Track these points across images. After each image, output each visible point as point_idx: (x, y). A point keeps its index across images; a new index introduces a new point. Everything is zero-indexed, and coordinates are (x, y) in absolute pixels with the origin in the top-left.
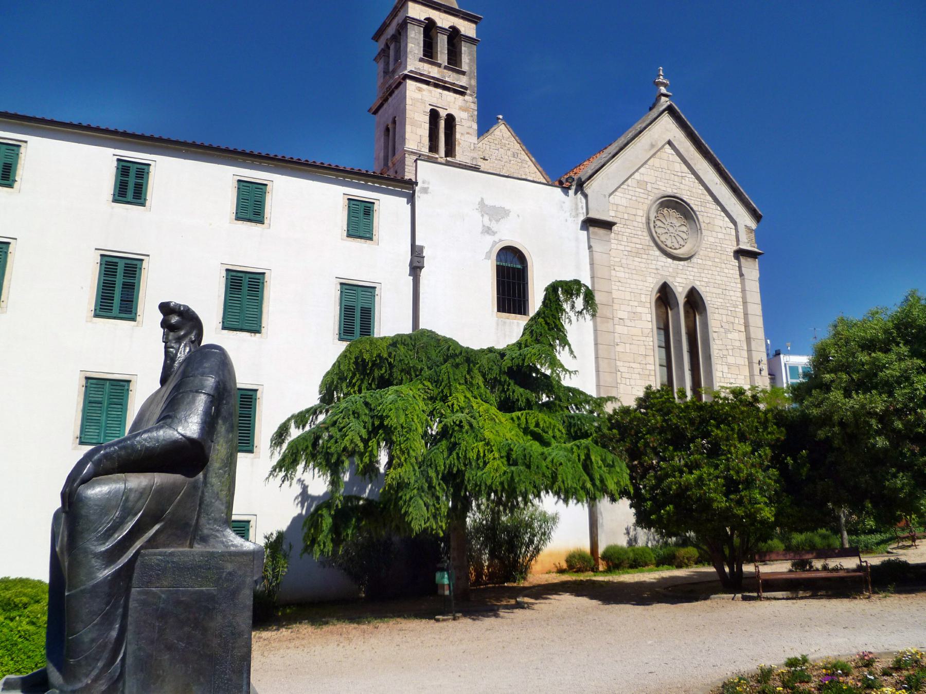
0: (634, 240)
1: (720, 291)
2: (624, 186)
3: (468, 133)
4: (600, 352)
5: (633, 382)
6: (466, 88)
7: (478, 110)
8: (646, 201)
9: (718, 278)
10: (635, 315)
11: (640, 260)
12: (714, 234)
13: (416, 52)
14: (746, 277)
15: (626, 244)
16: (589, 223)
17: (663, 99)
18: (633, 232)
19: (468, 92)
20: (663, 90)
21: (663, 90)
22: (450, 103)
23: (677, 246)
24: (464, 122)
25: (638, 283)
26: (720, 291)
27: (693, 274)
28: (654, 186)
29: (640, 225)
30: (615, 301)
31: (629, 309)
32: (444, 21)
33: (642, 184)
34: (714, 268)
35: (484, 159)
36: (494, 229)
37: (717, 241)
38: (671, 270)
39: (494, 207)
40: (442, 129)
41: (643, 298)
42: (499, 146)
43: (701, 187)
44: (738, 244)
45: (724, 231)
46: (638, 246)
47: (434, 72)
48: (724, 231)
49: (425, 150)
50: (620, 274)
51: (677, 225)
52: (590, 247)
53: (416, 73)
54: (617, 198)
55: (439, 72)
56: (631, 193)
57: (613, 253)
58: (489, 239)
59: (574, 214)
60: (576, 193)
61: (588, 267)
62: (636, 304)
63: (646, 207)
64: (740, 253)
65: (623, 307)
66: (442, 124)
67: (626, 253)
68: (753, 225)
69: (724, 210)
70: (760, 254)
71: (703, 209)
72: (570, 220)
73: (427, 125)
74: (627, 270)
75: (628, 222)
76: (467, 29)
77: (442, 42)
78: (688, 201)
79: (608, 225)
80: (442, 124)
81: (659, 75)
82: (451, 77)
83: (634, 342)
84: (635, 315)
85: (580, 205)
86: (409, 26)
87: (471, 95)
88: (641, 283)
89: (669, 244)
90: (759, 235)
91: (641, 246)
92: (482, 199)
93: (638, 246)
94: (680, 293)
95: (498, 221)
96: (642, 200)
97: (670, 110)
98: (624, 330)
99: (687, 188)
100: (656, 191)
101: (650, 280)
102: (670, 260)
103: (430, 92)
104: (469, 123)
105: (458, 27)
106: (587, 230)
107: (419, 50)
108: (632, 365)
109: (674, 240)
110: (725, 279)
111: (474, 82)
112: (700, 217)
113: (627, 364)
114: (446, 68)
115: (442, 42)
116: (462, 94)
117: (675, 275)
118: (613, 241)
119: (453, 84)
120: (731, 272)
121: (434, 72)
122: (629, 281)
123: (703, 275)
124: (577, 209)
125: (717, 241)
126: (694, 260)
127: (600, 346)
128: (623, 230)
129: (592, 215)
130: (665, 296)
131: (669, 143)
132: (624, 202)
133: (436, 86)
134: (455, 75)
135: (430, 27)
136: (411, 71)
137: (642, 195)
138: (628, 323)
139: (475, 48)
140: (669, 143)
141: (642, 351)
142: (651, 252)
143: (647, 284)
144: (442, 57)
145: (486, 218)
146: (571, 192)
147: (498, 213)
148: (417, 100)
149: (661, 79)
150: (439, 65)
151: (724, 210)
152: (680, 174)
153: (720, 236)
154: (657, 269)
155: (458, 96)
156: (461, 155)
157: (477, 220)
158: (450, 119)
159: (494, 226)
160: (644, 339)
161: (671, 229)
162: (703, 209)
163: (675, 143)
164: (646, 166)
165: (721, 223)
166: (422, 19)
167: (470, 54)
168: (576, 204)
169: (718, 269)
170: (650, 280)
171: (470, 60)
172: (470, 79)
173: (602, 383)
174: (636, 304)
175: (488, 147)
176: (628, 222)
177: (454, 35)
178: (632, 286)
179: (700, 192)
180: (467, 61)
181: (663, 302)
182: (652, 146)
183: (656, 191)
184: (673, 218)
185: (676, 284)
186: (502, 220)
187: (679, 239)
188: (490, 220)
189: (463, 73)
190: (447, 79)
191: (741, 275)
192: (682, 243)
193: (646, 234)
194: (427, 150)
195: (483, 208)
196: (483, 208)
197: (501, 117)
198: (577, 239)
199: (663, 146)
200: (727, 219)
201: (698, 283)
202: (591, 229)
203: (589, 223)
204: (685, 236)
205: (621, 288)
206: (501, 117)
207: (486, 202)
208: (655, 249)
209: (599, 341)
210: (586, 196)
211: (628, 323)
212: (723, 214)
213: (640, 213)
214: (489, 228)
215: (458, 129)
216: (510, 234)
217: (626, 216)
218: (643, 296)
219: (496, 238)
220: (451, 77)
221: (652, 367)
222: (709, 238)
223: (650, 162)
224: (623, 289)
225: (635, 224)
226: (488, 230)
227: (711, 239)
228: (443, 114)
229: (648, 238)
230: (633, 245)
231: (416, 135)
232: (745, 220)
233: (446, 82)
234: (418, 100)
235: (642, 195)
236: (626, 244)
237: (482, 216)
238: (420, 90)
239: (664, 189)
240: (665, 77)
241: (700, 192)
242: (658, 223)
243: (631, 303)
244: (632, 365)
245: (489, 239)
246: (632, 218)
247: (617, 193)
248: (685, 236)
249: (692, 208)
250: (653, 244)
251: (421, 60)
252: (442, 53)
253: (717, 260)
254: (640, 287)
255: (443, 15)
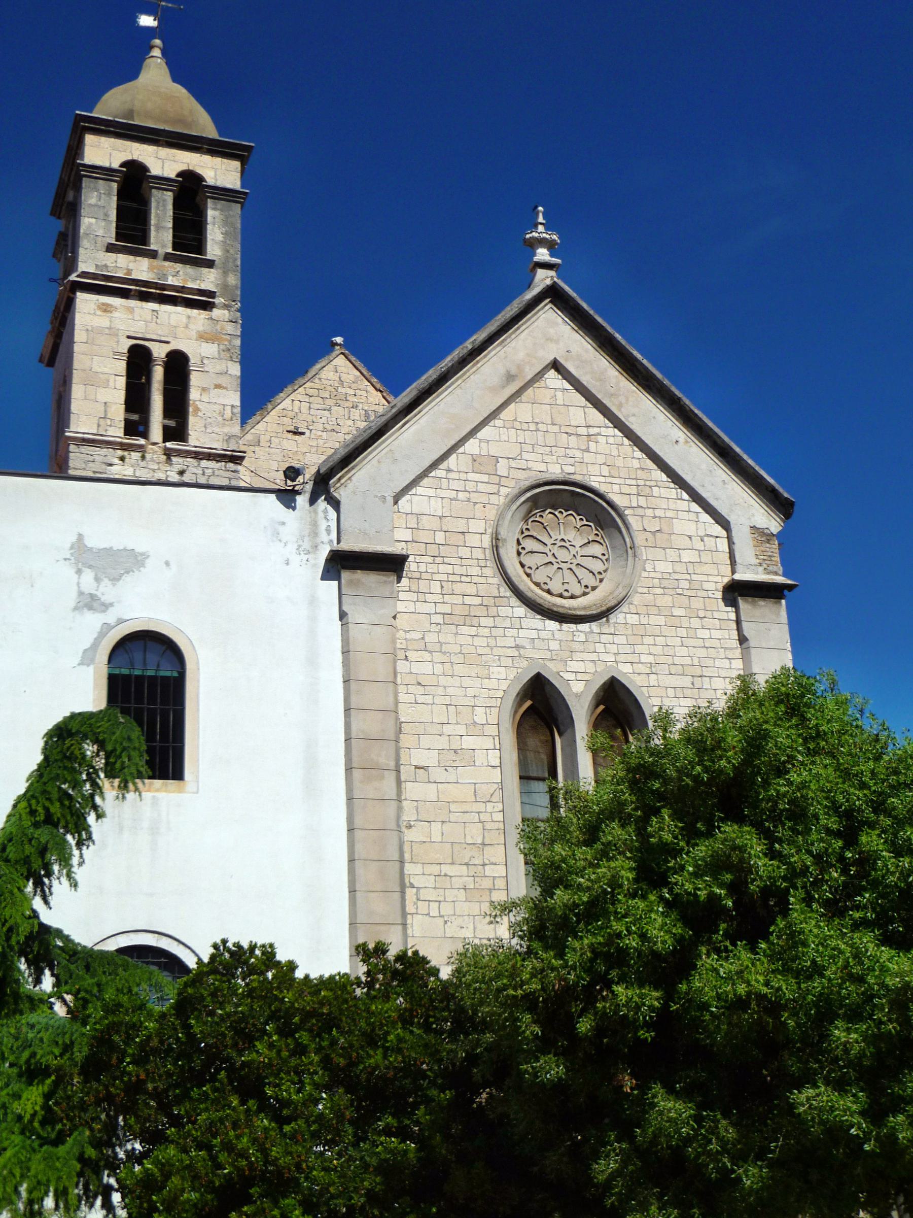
0: (458, 588)
1: (686, 681)
2: (439, 473)
3: (218, 386)
4: (358, 847)
5: (446, 909)
6: (212, 294)
7: (244, 336)
8: (494, 499)
9: (684, 651)
10: (456, 756)
11: (473, 631)
12: (672, 554)
13: (100, 232)
14: (752, 643)
15: (439, 598)
16: (341, 563)
17: (541, 273)
18: (458, 570)
19: (216, 301)
20: (542, 254)
21: (542, 254)
22: (171, 328)
23: (577, 590)
24: (209, 366)
25: (467, 682)
26: (686, 681)
27: (614, 648)
28: (514, 464)
29: (478, 554)
30: (406, 728)
31: (443, 743)
32: (165, 163)
33: (485, 464)
34: (671, 631)
35: (296, 433)
36: (105, 599)
37: (680, 568)
38: (554, 645)
39: (108, 551)
40: (157, 387)
41: (480, 716)
42: (329, 402)
43: (638, 454)
44: (733, 572)
45: (699, 545)
46: (468, 600)
47: (141, 269)
48: (699, 545)
49: (117, 432)
50: (421, 666)
51: (579, 542)
52: (343, 615)
53: (94, 276)
54: (421, 500)
55: (151, 268)
56: (455, 485)
57: (401, 622)
58: (93, 622)
59: (307, 545)
60: (313, 501)
61: (338, 658)
62: (461, 730)
63: (492, 514)
64: (736, 592)
65: (425, 741)
66: (158, 373)
67: (438, 619)
68: (773, 523)
69: (696, 497)
70: (790, 587)
71: (642, 501)
72: (296, 560)
73: (122, 382)
74: (438, 657)
75: (444, 551)
76: (220, 172)
77: (162, 212)
78: (602, 488)
79: (392, 564)
80: (158, 373)
81: (536, 225)
82: (178, 276)
83: (453, 817)
84: (456, 756)
85: (323, 525)
86: (85, 182)
87: (226, 307)
88: (477, 683)
89: (556, 587)
90: (787, 545)
91: (478, 601)
92: (80, 537)
93: (468, 600)
94: (577, 696)
95: (115, 580)
96: (484, 499)
97: (553, 294)
98: (430, 791)
99: (601, 459)
100: (522, 475)
101: (498, 672)
102: (552, 625)
103: (131, 310)
104: (220, 366)
105: (199, 171)
106: (338, 578)
107: (106, 229)
108: (445, 869)
109: (580, 572)
110: (702, 653)
111: (234, 280)
112: (631, 520)
113: (435, 869)
114: (168, 257)
115: (162, 212)
116: (206, 306)
117: (565, 655)
118: (402, 596)
119: (182, 289)
120: (716, 634)
121: (141, 269)
122: (443, 680)
123: (639, 649)
124: (314, 533)
125: (680, 568)
126: (617, 617)
127: (358, 834)
128: (432, 568)
129: (350, 544)
130: (540, 707)
131: (556, 365)
132: (436, 507)
133: (144, 297)
134: (189, 269)
135: (133, 182)
136: (84, 274)
137: (482, 487)
138: (438, 774)
139: (237, 209)
140: (556, 365)
141: (475, 834)
142: (503, 611)
143: (493, 684)
144: (161, 235)
145: (88, 577)
146: (302, 501)
147: (120, 563)
148: (100, 331)
149: (541, 232)
150: (153, 255)
151: (696, 497)
152: (583, 431)
153: (686, 556)
154: (518, 647)
155: (195, 312)
156: (200, 434)
157: (67, 581)
158: (178, 364)
159: (107, 592)
160: (481, 807)
161: (562, 555)
162: (642, 501)
163: (571, 367)
164: (498, 422)
165: (691, 528)
166: (115, 165)
167: (226, 222)
168: (315, 524)
169: (683, 632)
170: (498, 672)
171: (225, 234)
172: (225, 273)
173: (361, 918)
174: (461, 730)
175: (305, 406)
176: (444, 551)
177: (190, 190)
178: (451, 691)
179: (636, 464)
180: (220, 237)
181: (542, 718)
182: (510, 377)
183: (522, 475)
184: (569, 531)
185: (567, 676)
186: (127, 578)
187: (580, 572)
188: (97, 579)
189: (210, 264)
190: (171, 281)
191: (742, 640)
192: (592, 582)
193: (491, 570)
194: (121, 433)
195: (82, 555)
196: (82, 555)
197: (339, 340)
198: (313, 601)
199: (540, 375)
200: (706, 517)
201: (626, 669)
202: (345, 575)
203: (341, 563)
204: (597, 566)
205: (421, 699)
206: (339, 340)
207: (90, 543)
208: (514, 601)
209: (358, 822)
210: (335, 504)
211: (438, 774)
212: (695, 507)
213: (477, 526)
214: (93, 597)
215: (195, 380)
216: (142, 606)
217: (440, 538)
218: (479, 711)
219: (110, 617)
220: (178, 276)
221: (501, 871)
222: (656, 564)
223: (506, 414)
224: (429, 699)
225: (464, 552)
226: (90, 602)
227: (662, 567)
228: (159, 352)
229: (497, 580)
230: (458, 600)
231: (97, 398)
232: (751, 512)
233: (164, 287)
234: (102, 331)
235: (482, 487)
236: (439, 598)
237: (79, 572)
238: (106, 308)
239: (543, 467)
240: (548, 227)
241: (636, 464)
242: (529, 544)
243: (448, 730)
244: (445, 869)
245: (93, 622)
246: (457, 539)
247: (419, 490)
248: (597, 566)
249: (609, 503)
250: (509, 593)
251: (110, 248)
252: (159, 228)
253: (676, 612)
254: (471, 692)
255: (165, 152)
